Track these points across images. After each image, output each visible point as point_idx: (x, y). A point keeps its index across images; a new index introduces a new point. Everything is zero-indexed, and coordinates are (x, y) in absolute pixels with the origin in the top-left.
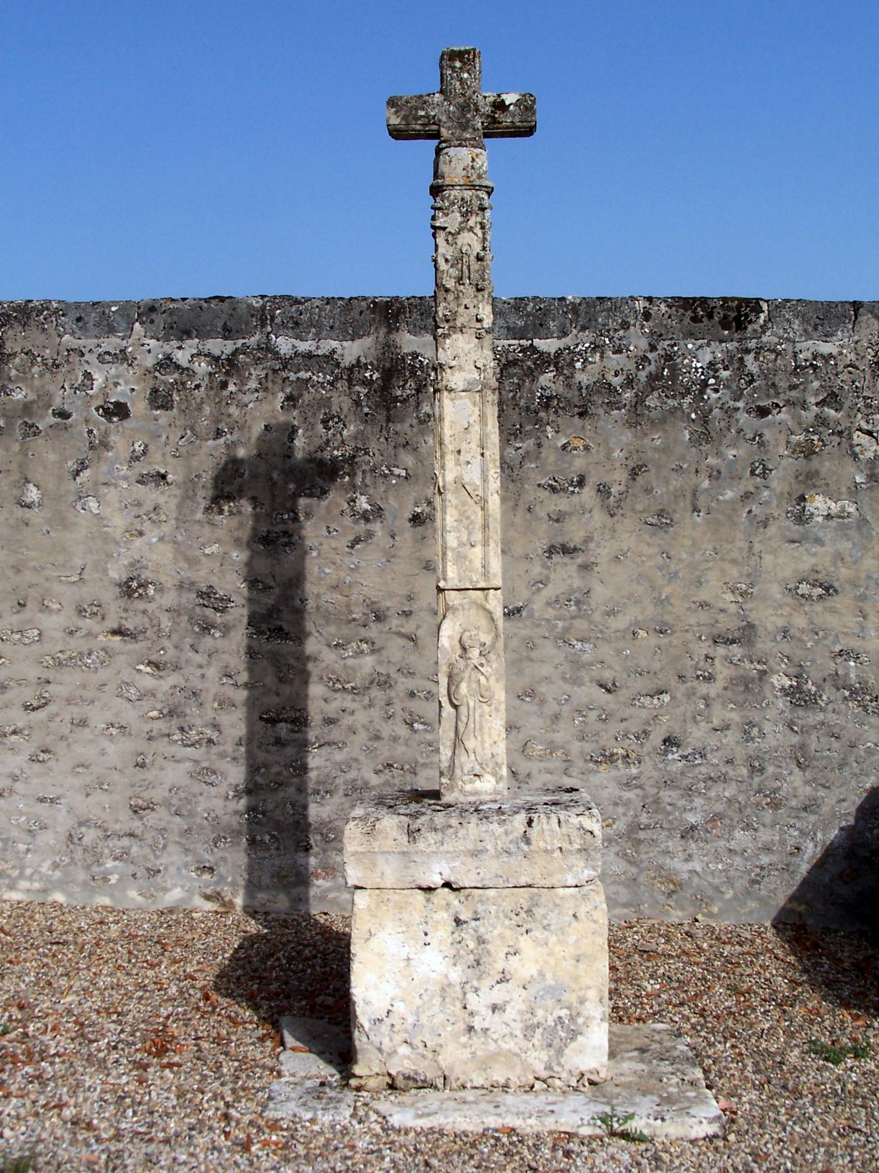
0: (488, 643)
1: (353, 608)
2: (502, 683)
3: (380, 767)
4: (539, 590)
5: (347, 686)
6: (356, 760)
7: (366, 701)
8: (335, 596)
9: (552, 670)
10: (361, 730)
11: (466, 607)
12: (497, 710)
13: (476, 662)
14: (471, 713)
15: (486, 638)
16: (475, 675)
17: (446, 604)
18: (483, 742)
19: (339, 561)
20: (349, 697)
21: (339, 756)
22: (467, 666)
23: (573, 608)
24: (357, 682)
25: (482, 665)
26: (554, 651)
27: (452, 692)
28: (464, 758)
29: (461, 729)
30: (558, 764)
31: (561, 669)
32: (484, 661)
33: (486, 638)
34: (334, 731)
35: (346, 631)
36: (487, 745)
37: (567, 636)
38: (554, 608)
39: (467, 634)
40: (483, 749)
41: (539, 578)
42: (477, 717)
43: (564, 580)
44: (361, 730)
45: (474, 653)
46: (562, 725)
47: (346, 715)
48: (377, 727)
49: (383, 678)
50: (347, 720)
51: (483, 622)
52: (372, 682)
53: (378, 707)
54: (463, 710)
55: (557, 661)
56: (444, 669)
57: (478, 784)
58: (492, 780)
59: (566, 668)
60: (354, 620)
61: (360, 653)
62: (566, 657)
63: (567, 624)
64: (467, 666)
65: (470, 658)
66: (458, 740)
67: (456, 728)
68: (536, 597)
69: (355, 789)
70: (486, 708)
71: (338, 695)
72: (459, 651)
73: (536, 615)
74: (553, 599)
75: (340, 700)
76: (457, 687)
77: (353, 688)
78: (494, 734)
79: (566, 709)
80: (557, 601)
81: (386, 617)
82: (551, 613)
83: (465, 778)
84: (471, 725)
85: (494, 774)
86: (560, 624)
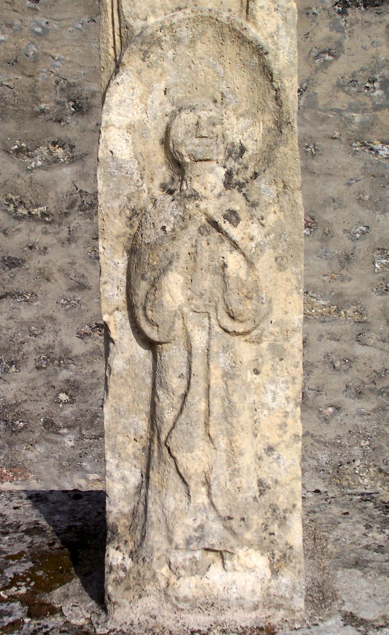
0: (252, 148)
1: (40, 94)
2: (293, 274)
3: (87, 329)
4: (326, 64)
5: (35, 211)
6: (52, 319)
7: (64, 234)
8: (13, 76)
9: (343, 188)
10: (57, 275)
11: (185, 33)
12: (279, 353)
13: (212, 206)
14: (198, 365)
15: (247, 131)
16: (210, 246)
17: (125, 26)
18: (233, 453)
19: (17, 23)
20: (40, 228)
21: (26, 313)
22: (185, 219)
23: (378, 92)
24: (50, 206)
25: (232, 217)
26: (346, 160)
27: (139, 299)
28: (174, 500)
29: (168, 416)
30: (348, 326)
31: (355, 186)
32: (238, 203)
33: (247, 131)
34: (19, 277)
35: (31, 129)
36: (246, 461)
37: (368, 136)
38: (347, 93)
39: (188, 118)
40: (235, 473)
41: (325, 46)
42: (216, 380)
43: (364, 48)
44: (57, 275)
45: (209, 179)
46: (356, 269)
47: (35, 254)
48: (82, 271)
49: (87, 200)
50: (36, 262)
51: (238, 81)
52: (71, 206)
53: (81, 242)
54: (174, 355)
55: (350, 174)
56: (114, 226)
57: (217, 578)
58: (259, 561)
59: (364, 185)
60: (43, 112)
61: (52, 162)
62: (365, 168)
63: (367, 117)
64: (185, 219)
65: (195, 196)
66: (157, 447)
67: (153, 405)
68: (321, 76)
69: (50, 359)
70: (245, 351)
71: (22, 225)
72: (163, 173)
73: (321, 103)
74: (348, 78)
75: (25, 231)
76: (155, 285)
77: (44, 215)
78: (268, 422)
79: (362, 245)
80: (353, 82)
81: (90, 107)
82: (342, 100)
83: (179, 558)
84: (198, 404)
85: (266, 545)
86: (357, 118)
